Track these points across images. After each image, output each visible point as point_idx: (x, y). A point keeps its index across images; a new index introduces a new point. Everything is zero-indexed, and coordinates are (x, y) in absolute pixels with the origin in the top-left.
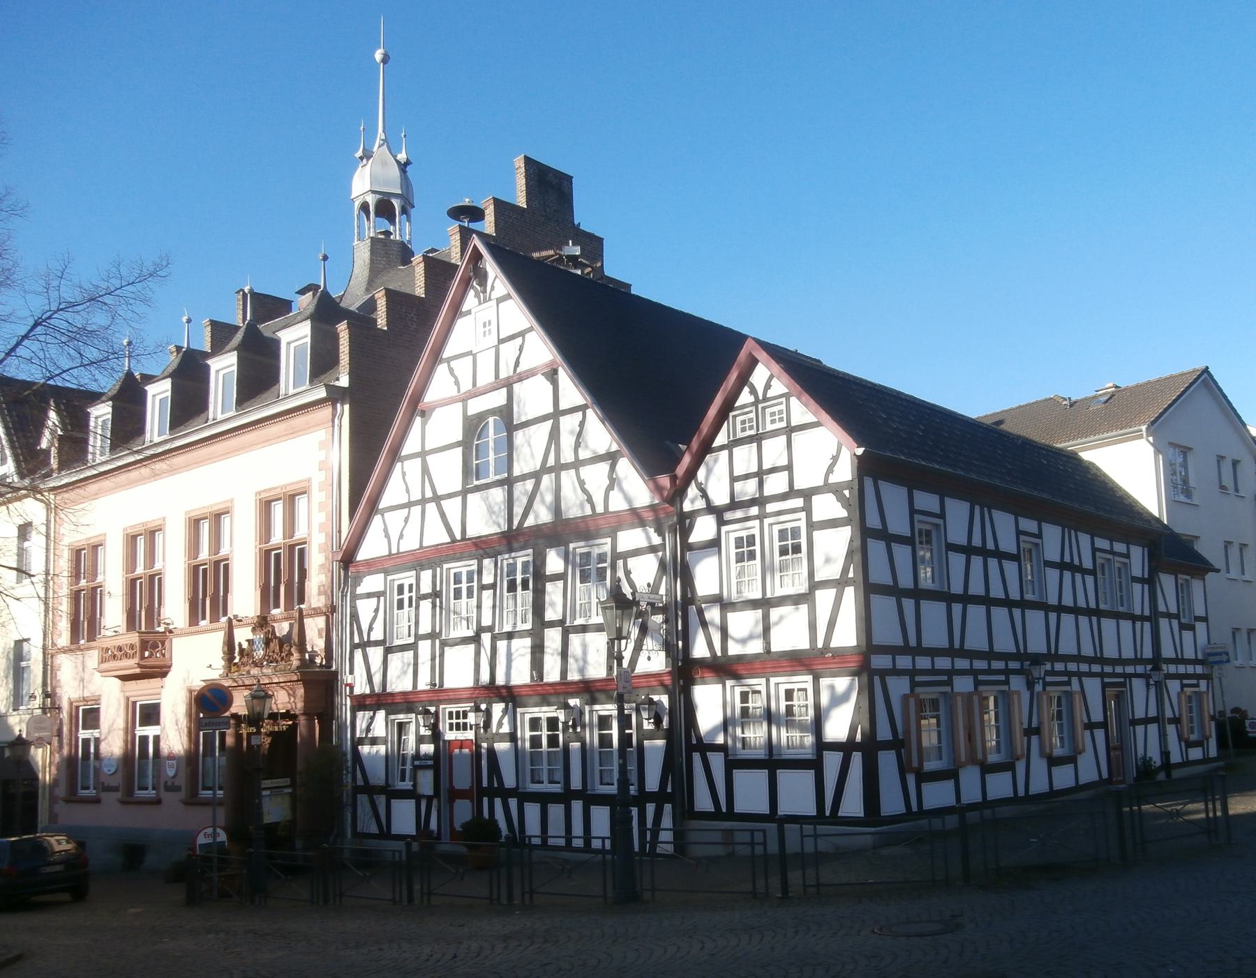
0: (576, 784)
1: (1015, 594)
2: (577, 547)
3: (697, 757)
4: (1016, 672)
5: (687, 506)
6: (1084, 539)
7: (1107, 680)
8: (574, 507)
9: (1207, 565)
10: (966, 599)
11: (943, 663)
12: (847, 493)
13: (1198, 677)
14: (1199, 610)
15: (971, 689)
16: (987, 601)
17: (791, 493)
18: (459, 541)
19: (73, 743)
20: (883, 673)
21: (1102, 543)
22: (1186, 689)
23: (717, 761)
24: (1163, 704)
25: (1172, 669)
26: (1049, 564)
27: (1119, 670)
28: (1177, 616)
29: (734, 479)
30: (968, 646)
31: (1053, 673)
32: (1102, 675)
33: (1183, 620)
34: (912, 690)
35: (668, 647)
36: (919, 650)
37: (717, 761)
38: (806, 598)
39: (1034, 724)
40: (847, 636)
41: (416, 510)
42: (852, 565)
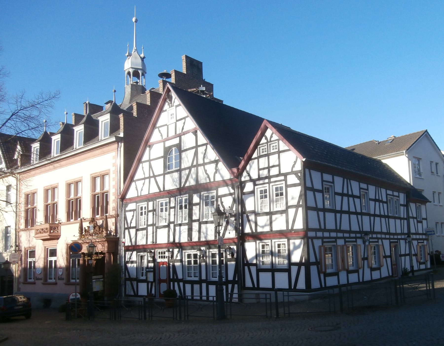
0: (204, 277)
1: (359, 210)
2: (204, 193)
3: (246, 268)
4: (359, 238)
5: (243, 179)
6: (383, 191)
7: (391, 241)
8: (203, 179)
9: (427, 200)
10: (342, 212)
11: (333, 234)
12: (299, 174)
13: (423, 239)
14: (424, 216)
15: (343, 244)
16: (349, 213)
17: (280, 174)
18: (162, 191)
19: (26, 263)
20: (312, 238)
21: (390, 192)
22: (419, 244)
23: (253, 269)
24: (411, 249)
25: (414, 237)
26: (371, 200)
27: (396, 237)
28: (416, 218)
29: (259, 170)
30: (342, 229)
31: (372, 238)
32: (389, 239)
33: (418, 220)
34: (322, 244)
35: (236, 229)
36: (325, 230)
37: (253, 269)
38: (285, 212)
39: (366, 256)
40: (299, 225)
41: (147, 180)
42: (301, 200)
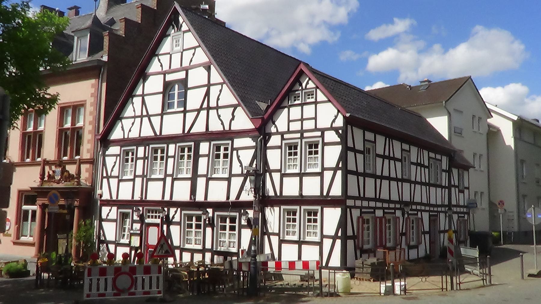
0: (208, 246)
1: (400, 176)
4: (398, 209)
6: (426, 153)
10: (382, 178)
11: (372, 204)
12: (340, 131)
13: (464, 213)
14: (466, 185)
15: (382, 215)
16: (389, 178)
17: (316, 129)
18: (159, 136)
20: (351, 207)
21: (432, 155)
22: (460, 218)
24: (451, 223)
25: (455, 209)
26: (413, 163)
27: (435, 209)
28: (458, 187)
29: (289, 121)
31: (412, 210)
32: (429, 211)
34: (361, 215)
36: (364, 199)
39: (404, 231)
40: (337, 191)
41: (138, 120)
42: (341, 162)
